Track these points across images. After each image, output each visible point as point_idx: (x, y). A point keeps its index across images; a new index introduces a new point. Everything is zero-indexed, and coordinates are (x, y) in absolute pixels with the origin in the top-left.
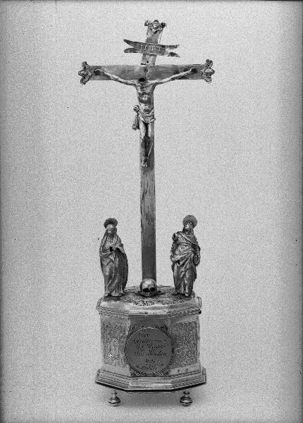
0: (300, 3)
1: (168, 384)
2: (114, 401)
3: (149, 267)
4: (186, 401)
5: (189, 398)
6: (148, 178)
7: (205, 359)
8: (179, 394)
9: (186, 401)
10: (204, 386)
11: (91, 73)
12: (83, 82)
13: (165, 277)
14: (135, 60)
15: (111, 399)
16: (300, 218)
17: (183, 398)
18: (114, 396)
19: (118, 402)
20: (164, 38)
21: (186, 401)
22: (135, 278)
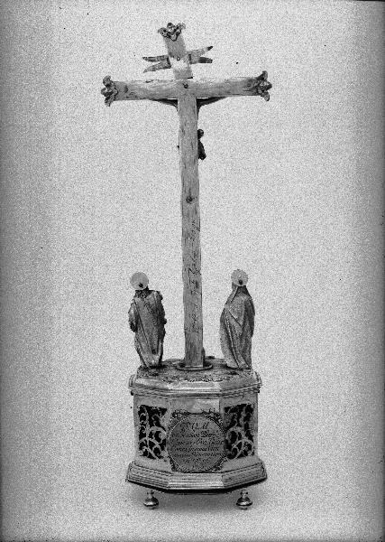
0: (380, 4)
1: (216, 481)
2: (151, 503)
3: (193, 329)
4: (244, 503)
5: (247, 499)
6: (191, 206)
7: (262, 452)
8: (235, 494)
9: (244, 503)
10: (263, 484)
11: (112, 92)
12: (264, 73)
13: (213, 346)
14: (167, 76)
15: (147, 500)
16: (379, 268)
17: (240, 500)
18: (150, 497)
19: (156, 504)
20: (191, 41)
21: (243, 503)
22: (174, 348)
